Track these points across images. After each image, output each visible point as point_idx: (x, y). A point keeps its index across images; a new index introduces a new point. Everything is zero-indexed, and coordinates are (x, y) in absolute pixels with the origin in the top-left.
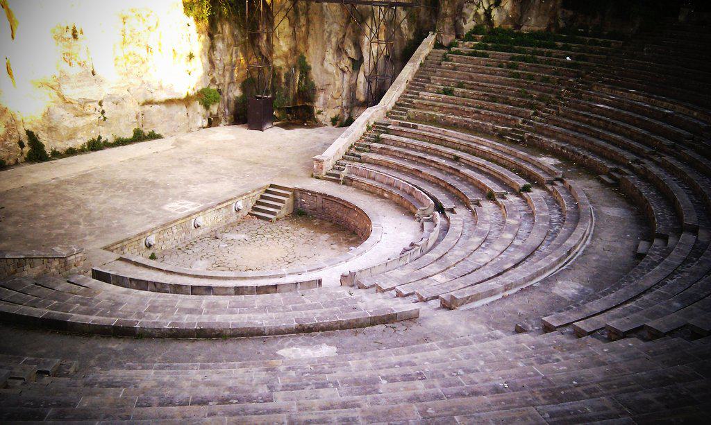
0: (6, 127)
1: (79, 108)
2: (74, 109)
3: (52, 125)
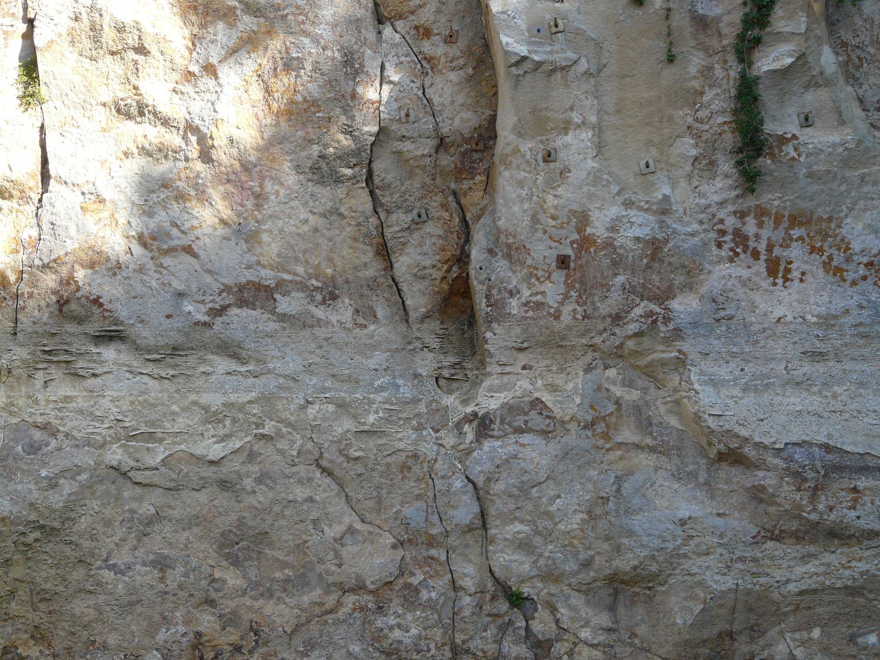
0: (400, 544)
1: (788, 493)
2: (757, 494)
3: (624, 563)
